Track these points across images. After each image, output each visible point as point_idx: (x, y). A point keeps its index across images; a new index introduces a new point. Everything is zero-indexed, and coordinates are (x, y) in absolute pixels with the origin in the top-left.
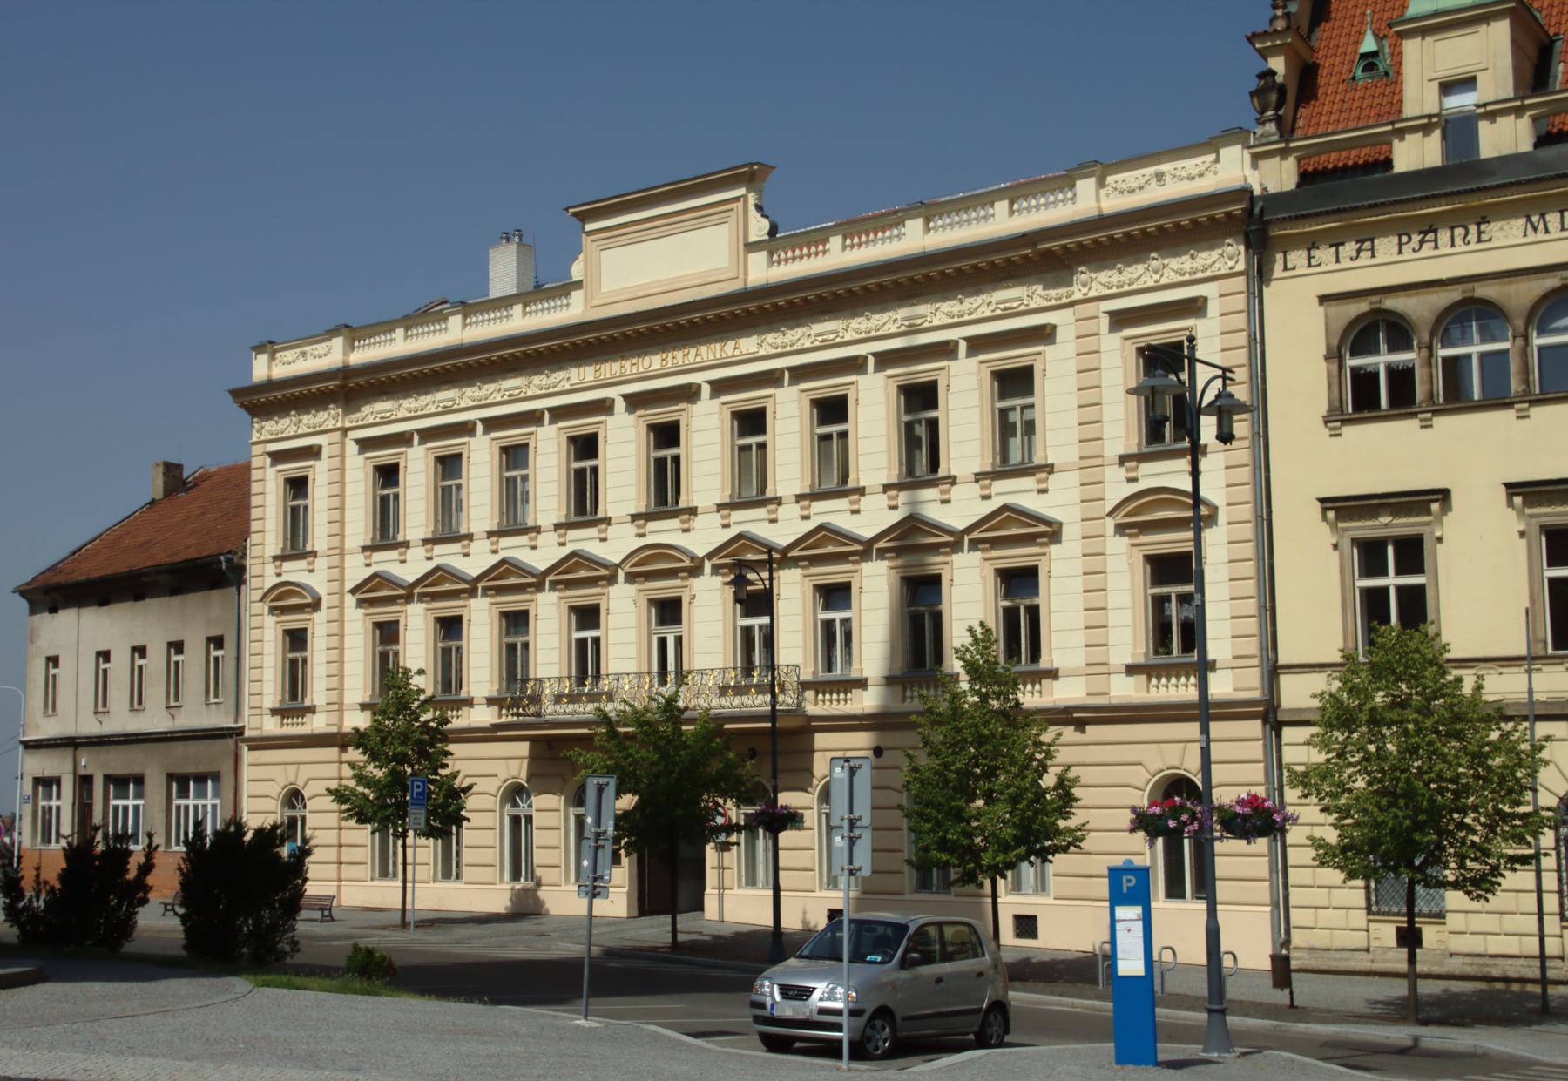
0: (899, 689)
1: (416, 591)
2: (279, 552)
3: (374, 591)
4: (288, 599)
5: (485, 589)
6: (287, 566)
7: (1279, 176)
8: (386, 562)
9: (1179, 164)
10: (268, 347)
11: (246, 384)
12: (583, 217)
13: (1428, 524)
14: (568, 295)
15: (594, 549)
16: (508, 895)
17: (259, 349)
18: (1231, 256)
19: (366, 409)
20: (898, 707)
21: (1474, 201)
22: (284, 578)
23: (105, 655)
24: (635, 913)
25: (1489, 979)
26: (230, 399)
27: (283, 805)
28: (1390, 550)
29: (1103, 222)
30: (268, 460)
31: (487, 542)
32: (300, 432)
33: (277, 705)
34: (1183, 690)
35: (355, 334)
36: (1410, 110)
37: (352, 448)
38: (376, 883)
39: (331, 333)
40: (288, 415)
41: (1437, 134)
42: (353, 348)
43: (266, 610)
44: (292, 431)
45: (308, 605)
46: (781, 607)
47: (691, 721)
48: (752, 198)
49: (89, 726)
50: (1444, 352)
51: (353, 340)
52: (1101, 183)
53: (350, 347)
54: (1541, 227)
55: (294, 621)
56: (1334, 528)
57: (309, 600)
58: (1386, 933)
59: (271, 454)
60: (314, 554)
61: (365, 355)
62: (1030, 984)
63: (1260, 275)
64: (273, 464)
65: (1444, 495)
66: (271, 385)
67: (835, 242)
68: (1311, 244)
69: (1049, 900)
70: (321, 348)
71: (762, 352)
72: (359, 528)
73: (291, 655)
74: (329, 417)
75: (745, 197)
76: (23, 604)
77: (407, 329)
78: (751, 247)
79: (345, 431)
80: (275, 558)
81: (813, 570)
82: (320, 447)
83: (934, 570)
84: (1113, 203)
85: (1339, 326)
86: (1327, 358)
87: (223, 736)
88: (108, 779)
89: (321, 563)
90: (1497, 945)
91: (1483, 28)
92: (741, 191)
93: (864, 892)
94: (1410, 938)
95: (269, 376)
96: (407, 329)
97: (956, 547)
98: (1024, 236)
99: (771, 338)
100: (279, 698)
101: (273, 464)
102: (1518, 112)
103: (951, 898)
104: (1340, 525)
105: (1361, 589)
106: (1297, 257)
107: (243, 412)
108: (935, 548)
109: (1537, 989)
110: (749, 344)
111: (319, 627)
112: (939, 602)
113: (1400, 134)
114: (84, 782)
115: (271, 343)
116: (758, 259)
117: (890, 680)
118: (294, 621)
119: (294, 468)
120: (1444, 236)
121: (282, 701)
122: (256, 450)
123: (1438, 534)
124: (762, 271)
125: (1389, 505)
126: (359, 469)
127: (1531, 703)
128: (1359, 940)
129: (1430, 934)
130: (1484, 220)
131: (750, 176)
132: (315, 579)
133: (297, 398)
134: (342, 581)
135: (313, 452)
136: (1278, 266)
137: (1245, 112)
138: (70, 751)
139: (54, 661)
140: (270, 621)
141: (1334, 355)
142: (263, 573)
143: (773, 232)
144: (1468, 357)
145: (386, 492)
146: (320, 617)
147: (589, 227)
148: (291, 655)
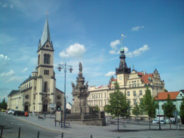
7: (108, 88)
8: (99, 99)
72: (104, 97)
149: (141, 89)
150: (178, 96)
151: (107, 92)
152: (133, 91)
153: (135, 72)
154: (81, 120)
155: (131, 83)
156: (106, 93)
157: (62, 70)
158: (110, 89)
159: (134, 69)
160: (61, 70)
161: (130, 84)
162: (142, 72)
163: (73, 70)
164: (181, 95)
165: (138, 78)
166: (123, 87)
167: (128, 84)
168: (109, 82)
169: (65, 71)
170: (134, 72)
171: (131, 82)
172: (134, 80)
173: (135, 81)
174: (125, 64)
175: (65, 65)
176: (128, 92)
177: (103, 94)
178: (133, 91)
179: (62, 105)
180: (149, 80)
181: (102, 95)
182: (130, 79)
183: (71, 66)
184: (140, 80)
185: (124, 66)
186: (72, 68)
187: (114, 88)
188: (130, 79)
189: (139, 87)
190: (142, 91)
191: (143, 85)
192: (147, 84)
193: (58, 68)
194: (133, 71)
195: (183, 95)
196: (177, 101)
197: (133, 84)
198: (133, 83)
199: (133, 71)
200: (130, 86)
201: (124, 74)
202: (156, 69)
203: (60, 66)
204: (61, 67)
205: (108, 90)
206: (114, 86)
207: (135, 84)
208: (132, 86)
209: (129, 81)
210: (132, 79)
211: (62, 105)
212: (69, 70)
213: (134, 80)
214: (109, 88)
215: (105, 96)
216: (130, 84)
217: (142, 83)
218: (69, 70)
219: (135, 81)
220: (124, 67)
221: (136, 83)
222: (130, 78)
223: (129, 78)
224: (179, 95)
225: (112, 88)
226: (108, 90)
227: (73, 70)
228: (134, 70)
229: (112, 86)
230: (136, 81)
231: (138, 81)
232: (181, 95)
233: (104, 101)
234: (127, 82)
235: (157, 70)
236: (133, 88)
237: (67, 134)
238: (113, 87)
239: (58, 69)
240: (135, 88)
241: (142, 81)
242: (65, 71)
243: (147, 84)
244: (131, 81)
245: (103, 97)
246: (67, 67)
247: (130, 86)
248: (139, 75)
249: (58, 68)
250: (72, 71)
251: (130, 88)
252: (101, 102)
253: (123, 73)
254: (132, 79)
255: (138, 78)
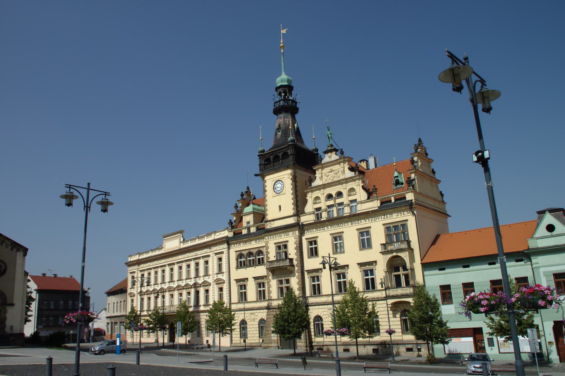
0: (195, 307)
1: (202, 285)
2: (217, 273)
3: (141, 293)
4: (132, 295)
5: (203, 286)
6: (219, 275)
7: (231, 235)
9: (222, 232)
10: (131, 256)
11: (127, 262)
12: (164, 237)
13: (374, 267)
14: (162, 249)
15: (208, 280)
16: (155, 340)
17: (129, 256)
18: (225, 246)
19: (141, 266)
20: (195, 310)
21: (249, 238)
22: (170, 286)
23: (114, 303)
24: (169, 342)
25: (251, 346)
26: (125, 264)
27: (206, 323)
28: (369, 272)
29: (215, 240)
30: (214, 255)
31: (202, 278)
32: (220, 249)
33: (204, 304)
34: (265, 304)
35: (140, 254)
36: (244, 226)
37: (139, 272)
38: (148, 338)
39: (137, 254)
40: (218, 246)
41: (246, 229)
42: (140, 256)
43: (215, 284)
44: (218, 249)
45: (223, 283)
46: (248, 287)
47: (160, 314)
48: (181, 235)
49: (113, 315)
50: (248, 259)
51: (140, 255)
52: (131, 258)
53: (139, 256)
54: (286, 235)
55: (220, 286)
56: (360, 268)
57: (223, 282)
58: (242, 340)
59: (215, 253)
60: (210, 275)
61: (141, 257)
62: (184, 350)
63: (229, 248)
64: (216, 255)
65: (347, 266)
66: (131, 262)
67: (151, 252)
68: (234, 244)
69: (209, 338)
70: (223, 232)
71: (182, 258)
72: (216, 271)
73: (220, 293)
74: (136, 267)
75: (180, 235)
76: (106, 295)
77: (207, 237)
78: (181, 242)
79: (138, 269)
80: (216, 274)
81: (205, 287)
82: (210, 255)
83: (198, 290)
84: (216, 237)
85: (237, 255)
86: (236, 260)
87: (124, 316)
88: (115, 323)
89: (211, 277)
90: (253, 341)
91: (250, 215)
92: (180, 234)
93: (192, 338)
94: (245, 341)
95: (214, 238)
96: (207, 237)
97: (200, 286)
98: (205, 242)
99: (183, 256)
100: (204, 303)
101: (216, 255)
102: (254, 226)
103: (224, 338)
104: (361, 268)
105: (312, 284)
106: (233, 246)
107: (127, 266)
108: (198, 287)
109: (244, 347)
110: (180, 257)
111: (135, 298)
112: (199, 295)
113: (243, 229)
114: (112, 323)
115: (131, 255)
116: (182, 244)
117: (194, 306)
118: (220, 286)
119: (219, 256)
120: (247, 243)
121: (205, 303)
122: (129, 272)
123: (347, 272)
124: (183, 246)
125: (367, 264)
126: (216, 258)
127: (244, 308)
128: (258, 341)
129: (247, 340)
130: (251, 241)
131: (181, 232)
132: (210, 280)
133: (216, 243)
134: (137, 292)
135: (209, 256)
136: (231, 247)
137: (228, 226)
138: (110, 319)
139: (109, 304)
140: (130, 298)
141: (237, 259)
142: (129, 291)
143: (184, 240)
144: (365, 239)
145: (250, 259)
146: (225, 285)
147: (165, 239)
148: (220, 293)
149: (364, 224)
150: (537, 235)
151: (225, 251)
152: (309, 257)
153: (337, 157)
154: (342, 294)
155: (323, 204)
156: (222, 253)
157: (78, 203)
158: (238, 237)
159: (332, 146)
160: (74, 201)
161: (317, 206)
162: (363, 161)
163: (112, 204)
164: (551, 228)
165: (347, 181)
166: (292, 221)
167: (309, 207)
168: (234, 211)
169: (87, 208)
170: (334, 157)
171: (323, 198)
172: (333, 191)
173: (340, 194)
174: (297, 133)
175: (89, 189)
176: (311, 243)
177: (210, 259)
178: (309, 257)
179: (13, 305)
180: (397, 183)
181: (207, 262)
182: (319, 188)
183: (106, 194)
184: (357, 185)
185: (291, 138)
186: (107, 197)
187: (253, 230)
188: (319, 188)
189: (355, 217)
190: (372, 231)
191: (375, 204)
192: (393, 200)
193: (62, 197)
194: (331, 151)
195: (559, 227)
196: (535, 260)
197: (329, 207)
198: (331, 202)
199: (326, 152)
200: (318, 216)
201: (294, 169)
202: (420, 140)
203: (72, 190)
204: (76, 193)
205: (228, 241)
206: (252, 223)
207: (341, 204)
208: (324, 216)
209: (317, 194)
210: (324, 186)
211: (13, 305)
212: (98, 203)
213: (333, 191)
214: (235, 234)
215: (220, 266)
216: (318, 209)
217: (368, 198)
218: (98, 203)
219: (340, 194)
220: (292, 141)
221: (345, 199)
222: (317, 182)
223: (314, 184)
224: (542, 231)
225: (245, 232)
226: (228, 241)
227: (112, 204)
228: (336, 150)
229: (245, 224)
230: (345, 193)
231: (352, 190)
232: (551, 228)
233: (216, 288)
234: (306, 202)
235: (425, 144)
236: (332, 221)
237: (428, 178)
238: (249, 229)
239: (64, 201)
240: (341, 220)
241: (370, 193)
242: (87, 208)
243: (393, 200)
244: (322, 194)
245: (210, 272)
246: (92, 194)
247: (318, 216)
248: (351, 169)
249: (62, 197)
250: (110, 207)
251: (319, 224)
252: (202, 291)
253: (287, 168)
254: (324, 186)
255: (347, 181)
